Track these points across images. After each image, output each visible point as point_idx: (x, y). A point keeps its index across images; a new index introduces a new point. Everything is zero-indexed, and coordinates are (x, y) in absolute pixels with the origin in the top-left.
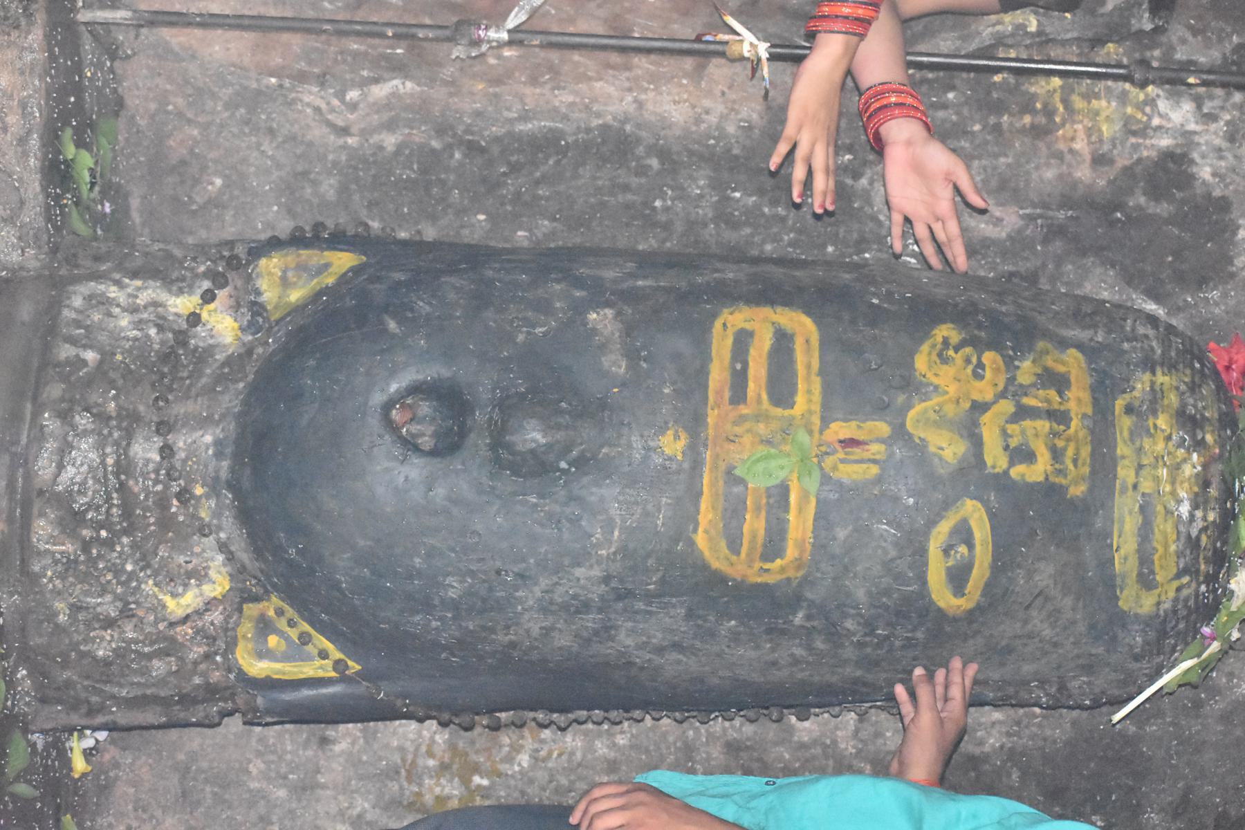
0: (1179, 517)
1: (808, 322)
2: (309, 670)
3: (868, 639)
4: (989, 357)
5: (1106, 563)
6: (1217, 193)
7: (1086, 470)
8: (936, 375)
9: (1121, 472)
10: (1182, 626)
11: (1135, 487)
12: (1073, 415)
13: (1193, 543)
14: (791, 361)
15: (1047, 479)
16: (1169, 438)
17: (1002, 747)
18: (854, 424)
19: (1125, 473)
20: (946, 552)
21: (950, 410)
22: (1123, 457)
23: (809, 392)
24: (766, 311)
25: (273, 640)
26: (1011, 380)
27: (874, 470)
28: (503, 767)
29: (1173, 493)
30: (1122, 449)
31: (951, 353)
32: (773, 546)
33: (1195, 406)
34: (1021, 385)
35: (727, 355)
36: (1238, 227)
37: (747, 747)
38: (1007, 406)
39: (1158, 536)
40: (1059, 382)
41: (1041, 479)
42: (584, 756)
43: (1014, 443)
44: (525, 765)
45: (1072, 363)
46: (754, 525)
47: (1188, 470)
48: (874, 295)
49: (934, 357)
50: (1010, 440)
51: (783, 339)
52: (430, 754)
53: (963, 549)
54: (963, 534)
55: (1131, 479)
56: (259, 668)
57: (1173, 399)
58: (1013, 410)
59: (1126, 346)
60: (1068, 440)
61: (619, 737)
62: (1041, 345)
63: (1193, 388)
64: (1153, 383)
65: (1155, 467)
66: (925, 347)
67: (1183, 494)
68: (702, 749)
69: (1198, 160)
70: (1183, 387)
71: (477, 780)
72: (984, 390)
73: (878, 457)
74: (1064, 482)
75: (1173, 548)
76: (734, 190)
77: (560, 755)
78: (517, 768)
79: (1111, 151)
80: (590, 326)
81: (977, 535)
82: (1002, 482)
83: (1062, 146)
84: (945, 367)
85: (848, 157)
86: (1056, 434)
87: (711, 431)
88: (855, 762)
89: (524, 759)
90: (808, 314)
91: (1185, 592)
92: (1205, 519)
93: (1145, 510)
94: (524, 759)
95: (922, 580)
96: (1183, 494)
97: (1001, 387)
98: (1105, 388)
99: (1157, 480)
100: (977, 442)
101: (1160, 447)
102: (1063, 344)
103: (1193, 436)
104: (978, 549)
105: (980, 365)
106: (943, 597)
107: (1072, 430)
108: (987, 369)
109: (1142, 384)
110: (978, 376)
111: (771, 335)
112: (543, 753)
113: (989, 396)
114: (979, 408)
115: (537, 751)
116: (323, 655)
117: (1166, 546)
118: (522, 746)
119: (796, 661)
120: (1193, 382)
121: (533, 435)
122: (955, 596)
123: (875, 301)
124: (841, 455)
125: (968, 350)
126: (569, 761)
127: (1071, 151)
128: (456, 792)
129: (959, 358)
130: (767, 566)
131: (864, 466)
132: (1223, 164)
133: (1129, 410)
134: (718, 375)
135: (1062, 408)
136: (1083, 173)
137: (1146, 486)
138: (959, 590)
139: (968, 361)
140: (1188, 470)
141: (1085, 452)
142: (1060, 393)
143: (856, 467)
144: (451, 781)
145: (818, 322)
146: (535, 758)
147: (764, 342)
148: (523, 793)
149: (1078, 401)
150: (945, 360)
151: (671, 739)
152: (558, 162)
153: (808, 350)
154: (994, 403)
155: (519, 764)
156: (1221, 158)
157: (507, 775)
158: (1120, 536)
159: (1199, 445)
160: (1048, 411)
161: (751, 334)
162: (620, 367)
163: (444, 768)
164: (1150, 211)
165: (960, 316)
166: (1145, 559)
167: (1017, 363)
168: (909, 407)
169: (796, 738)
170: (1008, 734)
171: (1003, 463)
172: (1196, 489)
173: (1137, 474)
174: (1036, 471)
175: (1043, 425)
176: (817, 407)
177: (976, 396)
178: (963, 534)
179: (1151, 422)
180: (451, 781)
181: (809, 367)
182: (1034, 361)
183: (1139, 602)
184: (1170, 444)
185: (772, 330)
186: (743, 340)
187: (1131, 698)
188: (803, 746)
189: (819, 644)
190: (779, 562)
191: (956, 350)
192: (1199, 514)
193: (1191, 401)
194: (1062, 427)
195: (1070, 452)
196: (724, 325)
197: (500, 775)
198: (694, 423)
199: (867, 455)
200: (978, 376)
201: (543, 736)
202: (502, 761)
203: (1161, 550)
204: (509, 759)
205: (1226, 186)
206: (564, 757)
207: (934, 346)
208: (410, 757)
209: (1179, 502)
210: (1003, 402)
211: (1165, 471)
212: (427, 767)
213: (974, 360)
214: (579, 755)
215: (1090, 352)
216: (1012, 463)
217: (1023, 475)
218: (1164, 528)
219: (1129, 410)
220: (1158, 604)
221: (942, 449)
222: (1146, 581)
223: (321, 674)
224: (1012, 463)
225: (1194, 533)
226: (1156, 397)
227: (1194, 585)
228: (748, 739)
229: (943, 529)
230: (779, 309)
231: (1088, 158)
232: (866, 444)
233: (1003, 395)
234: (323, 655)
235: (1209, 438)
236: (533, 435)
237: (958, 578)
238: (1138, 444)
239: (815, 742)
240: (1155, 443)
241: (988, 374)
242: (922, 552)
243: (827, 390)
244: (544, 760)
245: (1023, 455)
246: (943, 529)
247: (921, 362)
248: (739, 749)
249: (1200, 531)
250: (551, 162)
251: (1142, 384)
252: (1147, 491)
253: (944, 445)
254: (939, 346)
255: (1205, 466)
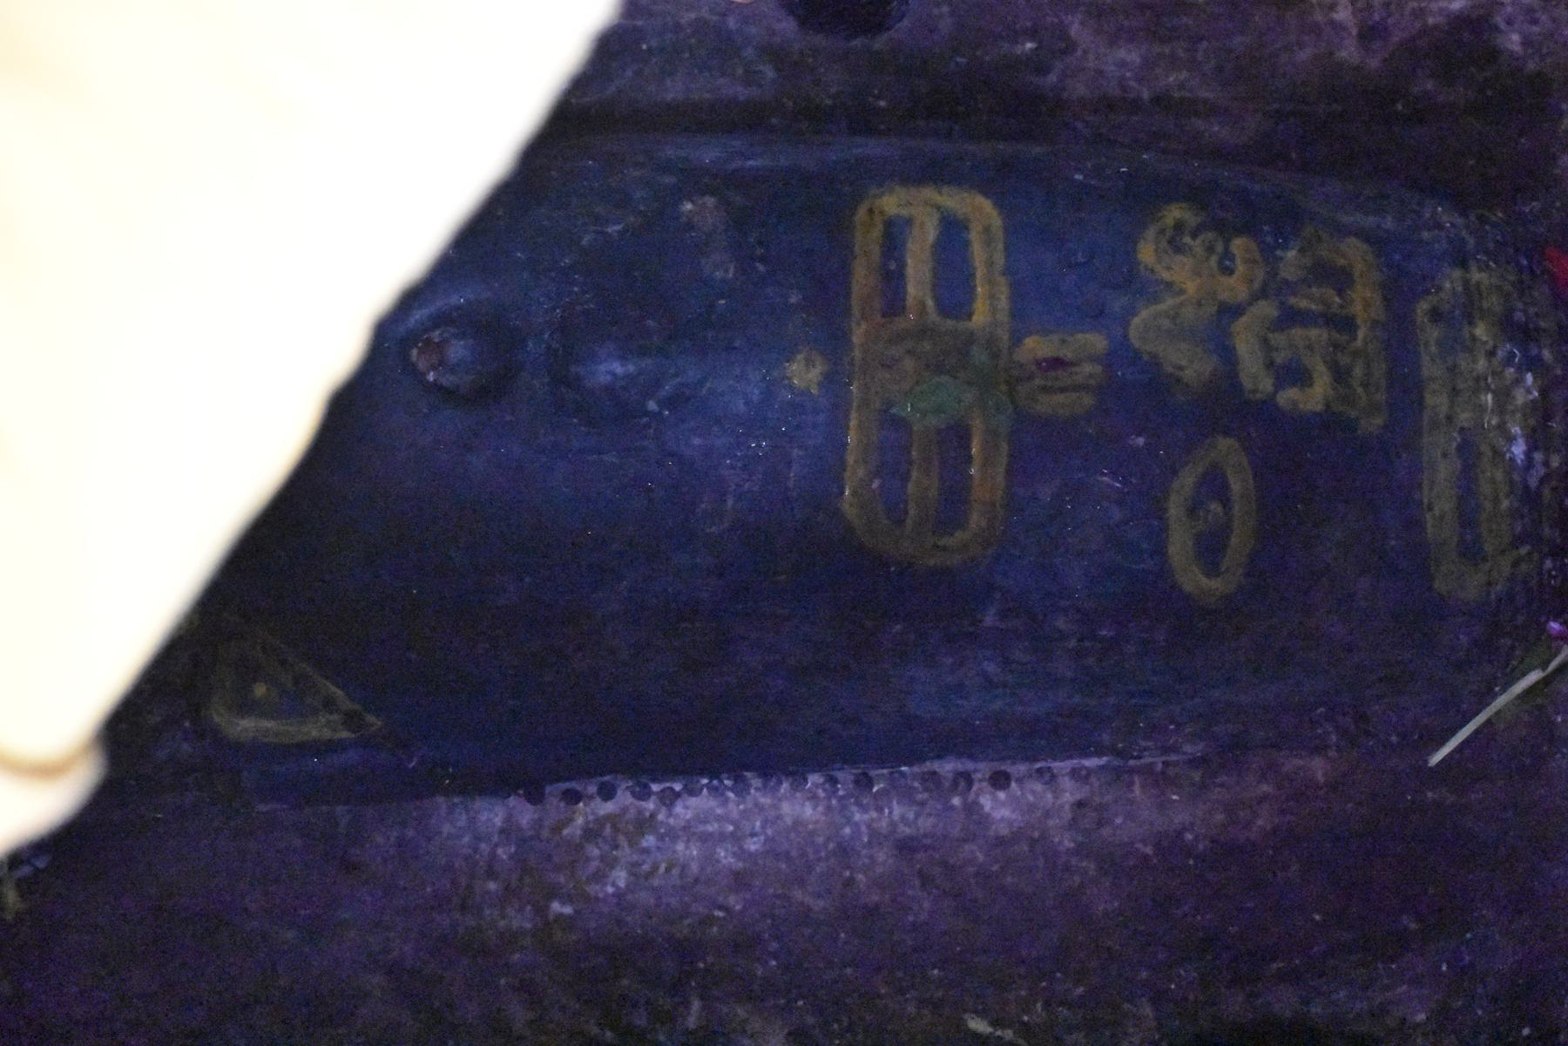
0: (1512, 460)
1: (986, 205)
2: (316, 729)
3: (1087, 644)
4: (1239, 245)
5: (1414, 524)
6: (1531, 66)
7: (1381, 397)
8: (1169, 268)
9: (1430, 400)
10: (1520, 619)
11: (1449, 418)
12: (1359, 322)
13: (1530, 498)
14: (966, 260)
15: (1328, 406)
16: (1491, 354)
17: (1274, 831)
18: (1055, 338)
19: (1437, 401)
20: (1193, 510)
21: (1189, 313)
22: (1432, 379)
23: (992, 297)
24: (929, 193)
25: (260, 690)
26: (1273, 274)
27: (1088, 400)
28: (593, 889)
29: (1502, 428)
30: (1430, 369)
31: (1187, 240)
32: (954, 500)
33: (1525, 312)
34: (1286, 282)
35: (876, 251)
36: (1561, 114)
37: (926, 848)
38: (1267, 309)
39: (1486, 488)
40: (1341, 279)
41: (1319, 408)
42: (702, 869)
43: (1280, 358)
44: (622, 884)
45: (1355, 253)
46: (922, 485)
47: (1520, 397)
48: (1078, 170)
49: (1164, 244)
50: (1275, 354)
51: (953, 229)
52: (491, 873)
53: (1215, 507)
54: (1214, 484)
55: (1444, 410)
56: (245, 727)
57: (1494, 303)
58: (1276, 313)
59: (1426, 235)
60: (1356, 354)
61: (749, 840)
62: (1308, 230)
63: (1522, 288)
64: (1466, 283)
65: (1476, 391)
66: (1151, 232)
67: (1516, 430)
68: (864, 852)
69: (1502, 26)
70: (1508, 287)
71: (556, 906)
72: (1234, 287)
73: (1092, 382)
74: (1353, 414)
75: (1505, 504)
76: (878, 98)
77: (668, 870)
78: (610, 890)
79: (1384, 19)
80: (684, 219)
81: (1236, 487)
82: (1265, 412)
83: (1319, 17)
84: (1179, 258)
85: (1029, 45)
86: (1336, 346)
87: (857, 353)
88: (1074, 861)
89: (621, 877)
90: (986, 195)
91: (1524, 567)
92: (1546, 464)
93: (1467, 449)
94: (621, 877)
95: (1160, 551)
96: (1516, 430)
97: (1257, 285)
98: (1401, 290)
99: (1481, 408)
100: (1227, 354)
101: (1482, 364)
102: (1342, 231)
103: (1525, 352)
104: (1236, 508)
105: (1227, 254)
106: (1192, 579)
107: (1359, 343)
108: (1238, 261)
109: (1451, 280)
110: (1228, 271)
111: (936, 222)
112: (646, 867)
113: (1242, 294)
114: (1231, 311)
115: (637, 864)
116: (329, 704)
117: (1496, 501)
118: (616, 859)
119: (989, 683)
120: (1521, 282)
121: (609, 369)
122: (1208, 576)
123: (1079, 177)
124: (1038, 382)
125: (1210, 235)
126: (682, 875)
127: (1332, 23)
128: (528, 926)
129: (1197, 245)
130: (945, 541)
131: (1074, 395)
132: (1536, 29)
133: (1436, 315)
134: (862, 278)
135: (1344, 312)
136: (1349, 52)
137: (1465, 417)
138: (1212, 569)
139: (1210, 249)
140: (1520, 397)
141: (1380, 369)
142: (1340, 292)
143: (1060, 398)
144: (521, 910)
145: (999, 204)
146: (633, 868)
147: (926, 232)
148: (619, 922)
149: (1364, 301)
150: (1179, 249)
151: (820, 840)
152: (638, 73)
153: (988, 242)
154: (1250, 304)
155: (613, 885)
156: (1535, 22)
157: (597, 899)
158: (1431, 489)
159: (1533, 363)
160: (1323, 315)
161: (909, 221)
162: (727, 271)
163: (509, 893)
164: (1441, 98)
165: (1195, 195)
166: (1467, 518)
167: (1279, 253)
168: (1131, 311)
169: (991, 833)
170: (1282, 812)
171: (1267, 384)
172: (1532, 422)
173: (1452, 402)
174: (1314, 397)
175: (1318, 334)
176: (1003, 317)
177: (1224, 296)
178: (1214, 484)
179: (1466, 329)
180: (521, 910)
181: (990, 264)
182: (1302, 250)
183: (1463, 584)
184: (1495, 362)
185: (937, 216)
186: (894, 236)
187: (1453, 732)
188: (1000, 841)
189: (1019, 654)
190: (959, 534)
191: (1194, 236)
192: (1538, 456)
193: (1520, 305)
194: (1345, 338)
195: (1358, 371)
196: (871, 211)
197: (587, 899)
198: (834, 342)
199: (1079, 379)
200: (1228, 271)
201: (644, 844)
202: (588, 881)
203: (1488, 505)
204: (599, 877)
205: (1543, 58)
206: (675, 872)
207: (1162, 231)
208: (463, 881)
209: (1511, 439)
210: (1262, 303)
211: (1490, 397)
212: (488, 892)
213: (1220, 248)
214: (695, 867)
215: (1377, 241)
216: (1279, 385)
217: (1295, 403)
218: (1491, 477)
219: (1436, 315)
220: (1489, 584)
221: (1181, 368)
222: (1471, 552)
223: (327, 734)
224: (1279, 385)
225: (1533, 482)
226: (1471, 294)
227: (1536, 556)
228: (925, 836)
229: (1187, 481)
230: (945, 189)
231: (1354, 32)
232: (1072, 364)
233: (1263, 293)
234: (329, 704)
235: (1547, 354)
236: (609, 369)
237: (1210, 550)
238: (1450, 361)
239: (1016, 836)
240: (1475, 362)
241: (1241, 268)
242: (1160, 512)
243: (1018, 293)
244: (649, 875)
245: (1295, 374)
246: (1187, 481)
247: (1146, 253)
248: (913, 850)
249: (1542, 481)
250: (629, 73)
251: (1451, 280)
252: (1466, 425)
253: (1184, 363)
254: (1169, 233)
255: (1544, 392)
